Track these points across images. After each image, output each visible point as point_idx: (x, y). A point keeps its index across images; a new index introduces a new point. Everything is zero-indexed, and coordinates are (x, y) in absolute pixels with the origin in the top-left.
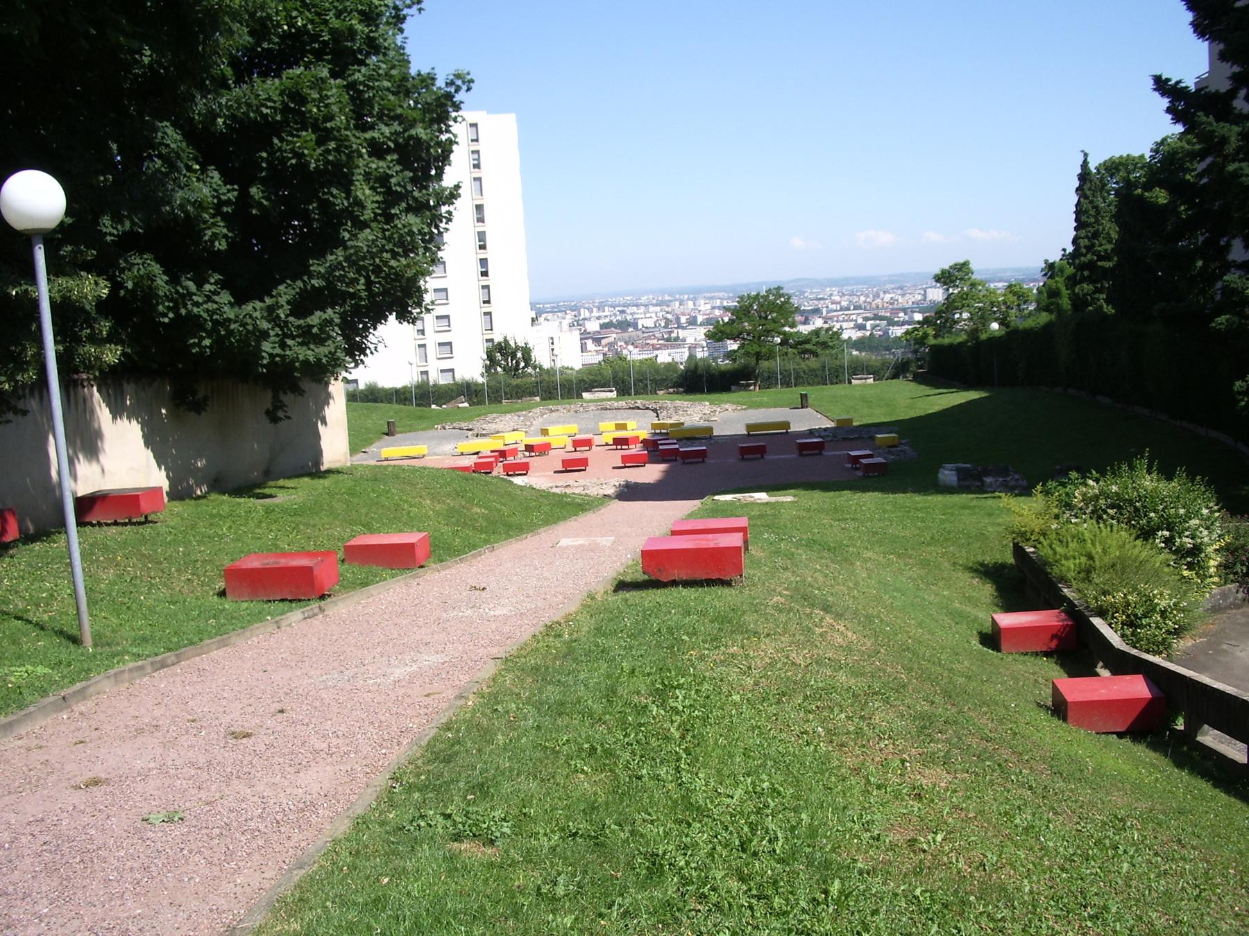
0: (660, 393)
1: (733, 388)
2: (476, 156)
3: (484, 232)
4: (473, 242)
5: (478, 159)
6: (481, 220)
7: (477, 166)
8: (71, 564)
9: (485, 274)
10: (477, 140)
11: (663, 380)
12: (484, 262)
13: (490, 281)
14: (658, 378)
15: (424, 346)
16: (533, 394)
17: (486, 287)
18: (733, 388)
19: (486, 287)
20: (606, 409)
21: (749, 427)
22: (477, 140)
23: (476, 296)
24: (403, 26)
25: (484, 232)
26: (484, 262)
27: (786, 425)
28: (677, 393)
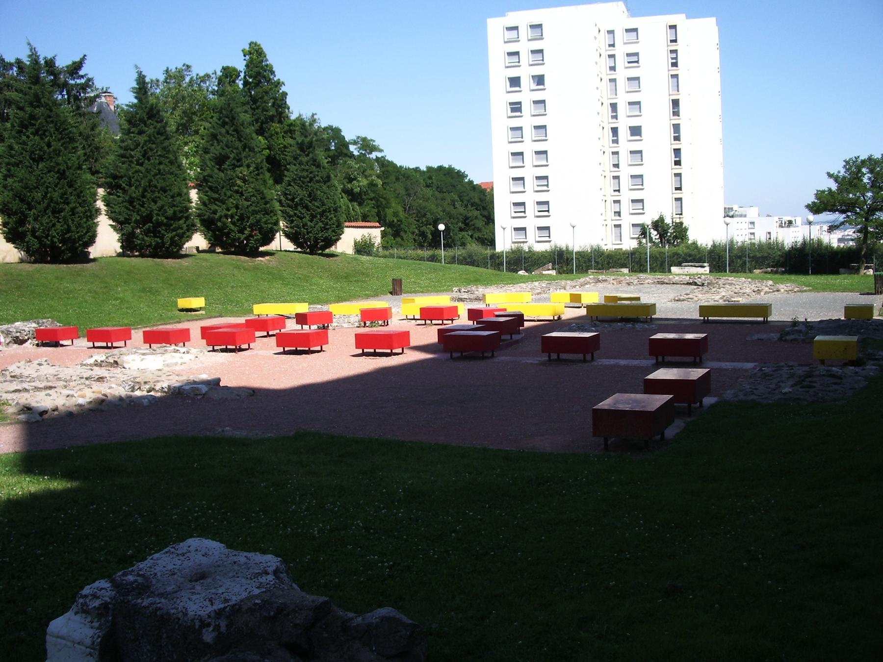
0: (757, 271)
1: (841, 270)
2: (674, 56)
3: (617, 128)
4: (669, 133)
5: (676, 58)
6: (676, 113)
7: (675, 65)
8: (221, 316)
9: (678, 163)
10: (675, 41)
11: (764, 258)
12: (677, 152)
13: (683, 170)
14: (758, 255)
15: (619, 226)
16: (624, 266)
17: (678, 175)
18: (841, 270)
19: (678, 175)
20: (663, 283)
21: (703, 310)
22: (675, 41)
23: (669, 182)
24: (62, 63)
25: (617, 128)
26: (677, 152)
27: (763, 309)
28: (776, 272)
